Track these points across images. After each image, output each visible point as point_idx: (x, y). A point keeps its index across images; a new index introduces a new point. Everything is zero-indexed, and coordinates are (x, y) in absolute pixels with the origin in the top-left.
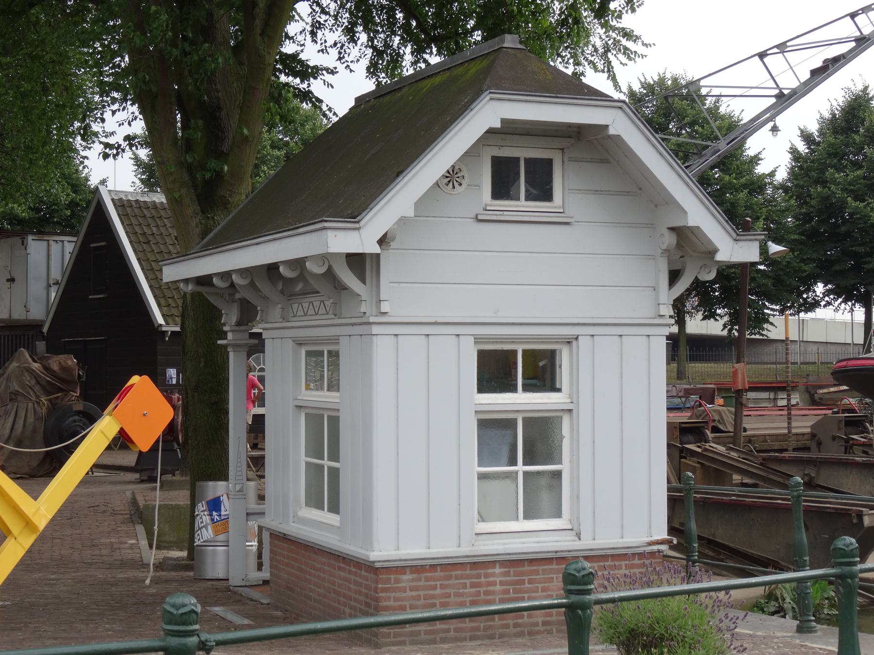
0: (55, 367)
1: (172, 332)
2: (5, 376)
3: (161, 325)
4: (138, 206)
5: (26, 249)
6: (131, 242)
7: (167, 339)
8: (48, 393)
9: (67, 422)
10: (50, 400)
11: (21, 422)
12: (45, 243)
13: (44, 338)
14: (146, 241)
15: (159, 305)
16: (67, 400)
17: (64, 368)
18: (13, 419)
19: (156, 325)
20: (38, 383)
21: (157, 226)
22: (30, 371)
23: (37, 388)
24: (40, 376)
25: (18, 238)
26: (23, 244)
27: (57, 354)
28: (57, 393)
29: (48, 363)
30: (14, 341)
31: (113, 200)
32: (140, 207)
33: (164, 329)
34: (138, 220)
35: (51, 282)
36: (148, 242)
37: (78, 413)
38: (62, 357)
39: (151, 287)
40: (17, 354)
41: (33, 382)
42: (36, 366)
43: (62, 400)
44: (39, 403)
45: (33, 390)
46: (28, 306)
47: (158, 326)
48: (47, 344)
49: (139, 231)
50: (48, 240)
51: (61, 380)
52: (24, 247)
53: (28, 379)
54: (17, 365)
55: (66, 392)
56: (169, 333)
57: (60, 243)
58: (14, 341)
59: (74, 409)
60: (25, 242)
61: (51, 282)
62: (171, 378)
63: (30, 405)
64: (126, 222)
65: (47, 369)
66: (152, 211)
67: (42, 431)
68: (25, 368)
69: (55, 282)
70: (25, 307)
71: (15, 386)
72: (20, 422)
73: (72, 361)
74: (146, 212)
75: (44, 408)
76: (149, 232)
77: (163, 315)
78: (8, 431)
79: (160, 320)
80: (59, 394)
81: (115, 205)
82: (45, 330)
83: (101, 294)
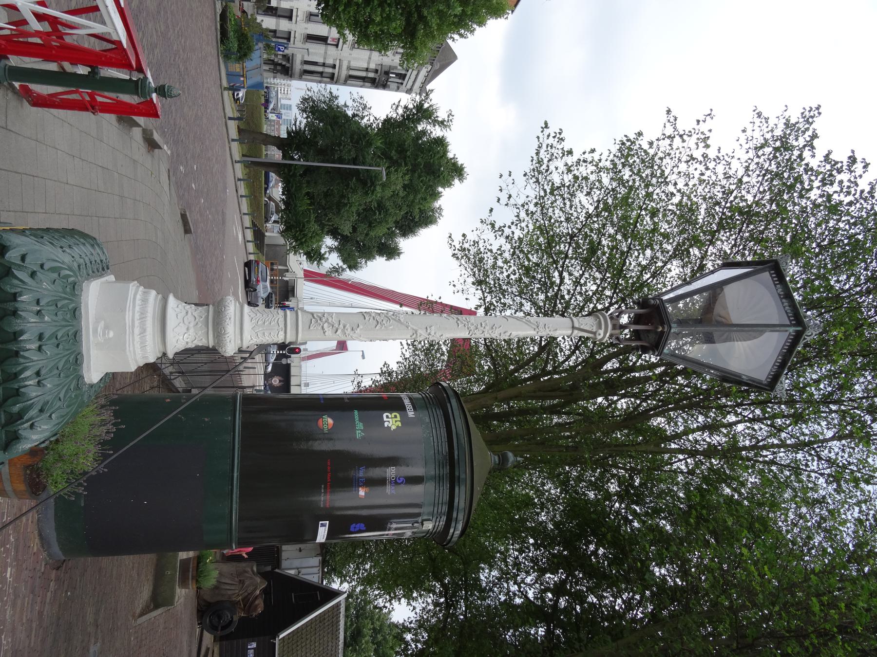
0: (257, 602)
2: (253, 576)
8: (243, 600)
10: (239, 601)
11: (228, 588)
13: (273, 569)
17: (256, 607)
20: (249, 594)
22: (255, 590)
23: (246, 594)
27: (264, 602)
36: (320, 622)
37: (232, 618)
39: (298, 628)
40: (264, 581)
41: (249, 592)
42: (258, 592)
51: (250, 606)
53: (251, 588)
55: (244, 610)
63: (237, 591)
65: (256, 598)
73: (260, 610)
74: (335, 618)
76: (325, 621)
79: (281, 636)
82: (277, 570)
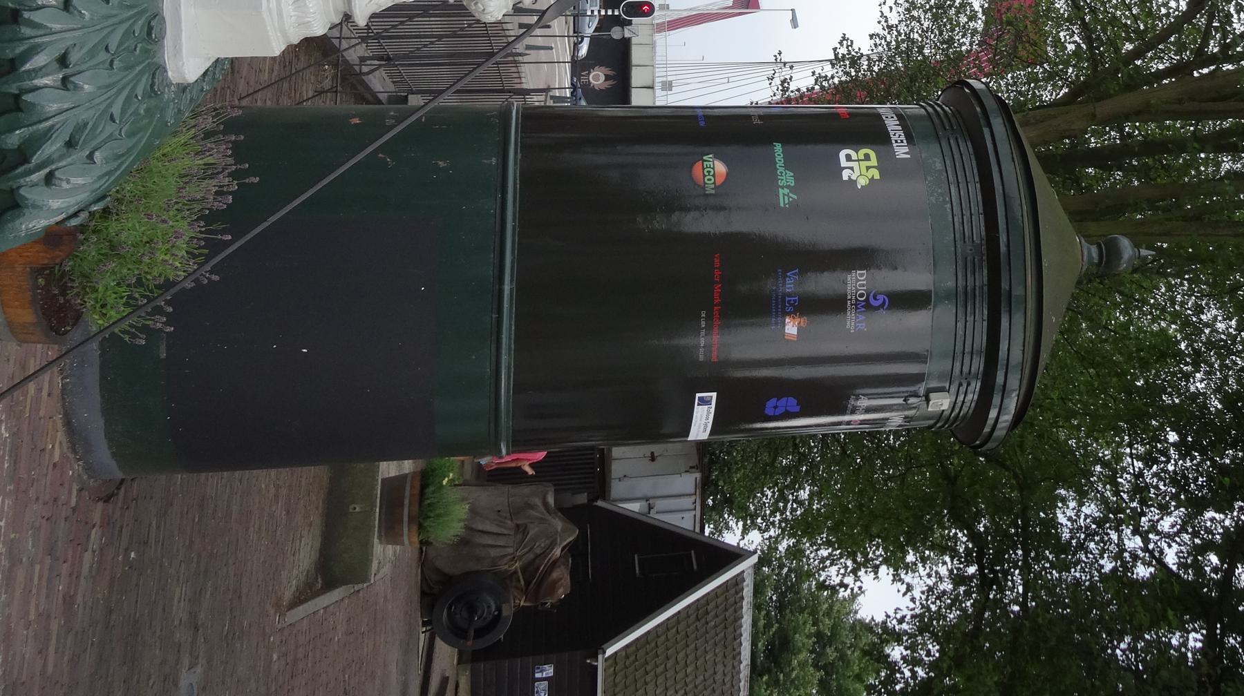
0: (555, 575)
1: (596, 667)
2: (547, 516)
3: (605, 653)
4: (737, 600)
5: (686, 471)
6: (698, 600)
7: (588, 661)
8: (524, 569)
9: (488, 598)
10: (515, 572)
11: (490, 542)
12: (693, 491)
14: (699, 617)
15: (627, 646)
16: (516, 594)
17: (553, 586)
18: (495, 531)
19: (604, 646)
20: (537, 556)
21: (716, 626)
22: (552, 546)
23: (531, 556)
24: (546, 556)
25: (697, 461)
26: (691, 467)
28: (524, 578)
29: (560, 566)
30: (581, 462)
31: (743, 572)
32: (736, 603)
33: (600, 657)
34: (722, 604)
35: (651, 501)
36: (698, 619)
37: (499, 609)
38: (567, 580)
39: (649, 632)
41: (538, 551)
42: (557, 552)
43: (517, 588)
44: (512, 561)
45: (527, 552)
46: (625, 479)
47: (603, 649)
48: (583, 505)
49: (709, 607)
50: (695, 494)
52: (688, 469)
53: (542, 544)
54: (559, 530)
56: (596, 664)
57: (693, 507)
58: (581, 462)
59: (504, 605)
60: (693, 470)
61: (651, 501)
62: (542, 671)
63: (510, 550)
64: (719, 591)
65: (554, 564)
66: (732, 617)
67: (479, 568)
68: (556, 540)
69: (652, 505)
70: (625, 476)
71: (533, 531)
72: (489, 541)
73: (561, 593)
74: (731, 610)
75: (506, 567)
77: (616, 653)
78: (480, 527)
79: (610, 651)
80: (522, 582)
81: (738, 575)
82: (600, 503)
83: (639, 570)
